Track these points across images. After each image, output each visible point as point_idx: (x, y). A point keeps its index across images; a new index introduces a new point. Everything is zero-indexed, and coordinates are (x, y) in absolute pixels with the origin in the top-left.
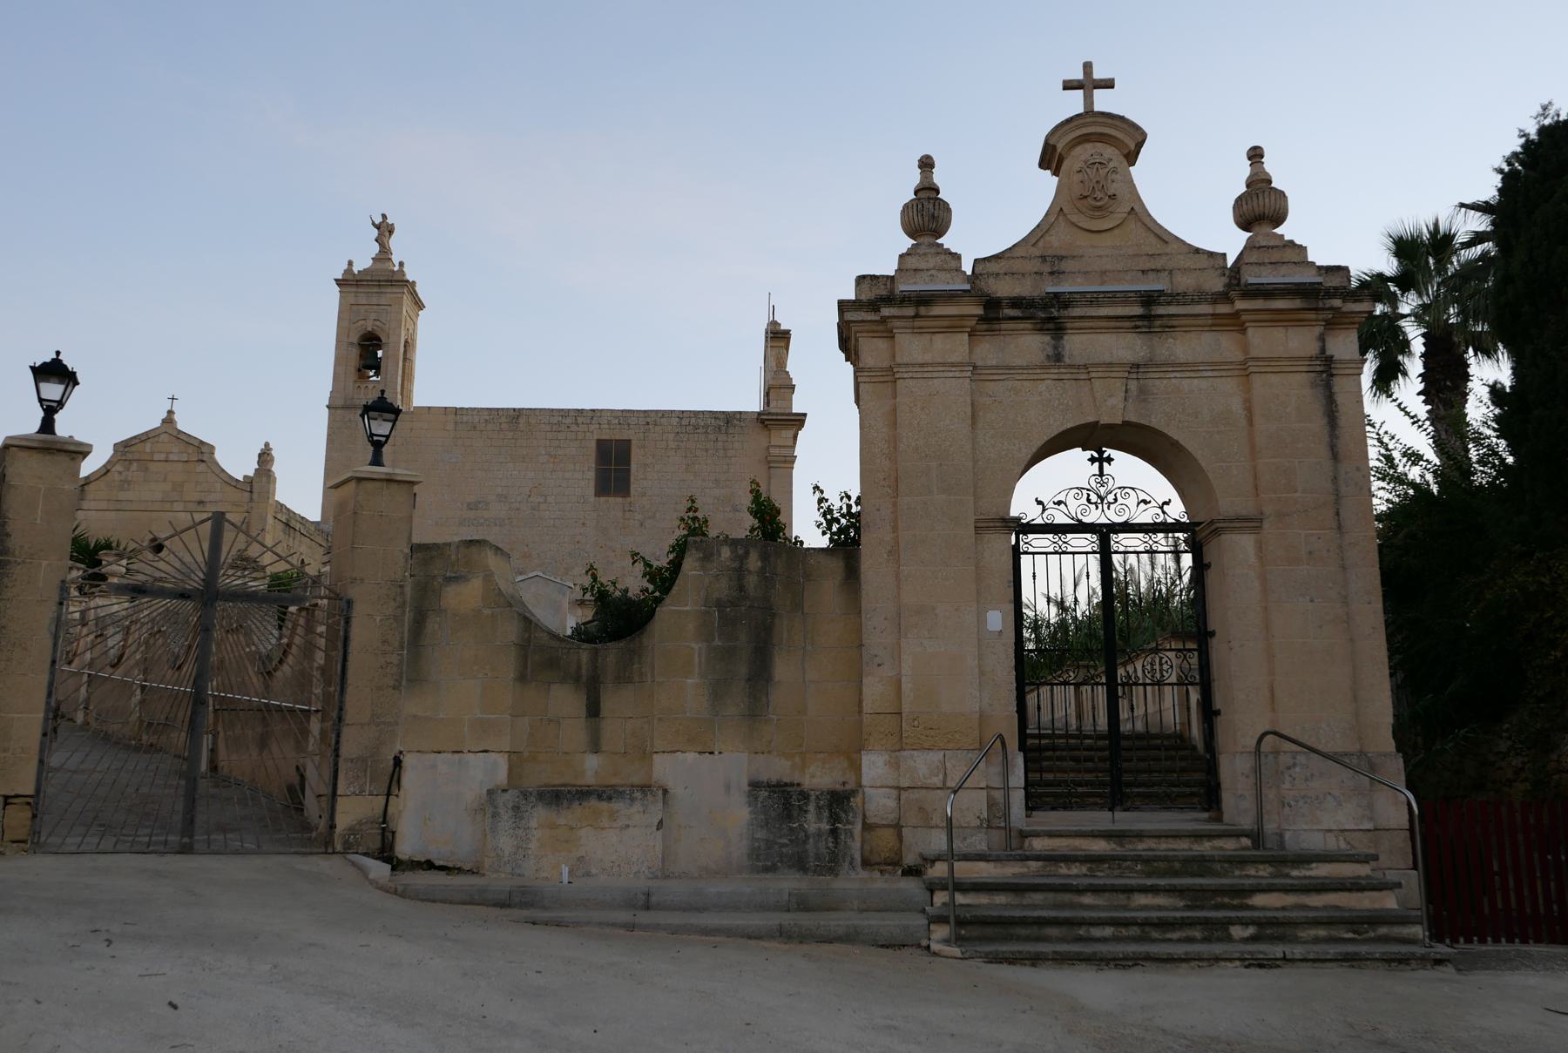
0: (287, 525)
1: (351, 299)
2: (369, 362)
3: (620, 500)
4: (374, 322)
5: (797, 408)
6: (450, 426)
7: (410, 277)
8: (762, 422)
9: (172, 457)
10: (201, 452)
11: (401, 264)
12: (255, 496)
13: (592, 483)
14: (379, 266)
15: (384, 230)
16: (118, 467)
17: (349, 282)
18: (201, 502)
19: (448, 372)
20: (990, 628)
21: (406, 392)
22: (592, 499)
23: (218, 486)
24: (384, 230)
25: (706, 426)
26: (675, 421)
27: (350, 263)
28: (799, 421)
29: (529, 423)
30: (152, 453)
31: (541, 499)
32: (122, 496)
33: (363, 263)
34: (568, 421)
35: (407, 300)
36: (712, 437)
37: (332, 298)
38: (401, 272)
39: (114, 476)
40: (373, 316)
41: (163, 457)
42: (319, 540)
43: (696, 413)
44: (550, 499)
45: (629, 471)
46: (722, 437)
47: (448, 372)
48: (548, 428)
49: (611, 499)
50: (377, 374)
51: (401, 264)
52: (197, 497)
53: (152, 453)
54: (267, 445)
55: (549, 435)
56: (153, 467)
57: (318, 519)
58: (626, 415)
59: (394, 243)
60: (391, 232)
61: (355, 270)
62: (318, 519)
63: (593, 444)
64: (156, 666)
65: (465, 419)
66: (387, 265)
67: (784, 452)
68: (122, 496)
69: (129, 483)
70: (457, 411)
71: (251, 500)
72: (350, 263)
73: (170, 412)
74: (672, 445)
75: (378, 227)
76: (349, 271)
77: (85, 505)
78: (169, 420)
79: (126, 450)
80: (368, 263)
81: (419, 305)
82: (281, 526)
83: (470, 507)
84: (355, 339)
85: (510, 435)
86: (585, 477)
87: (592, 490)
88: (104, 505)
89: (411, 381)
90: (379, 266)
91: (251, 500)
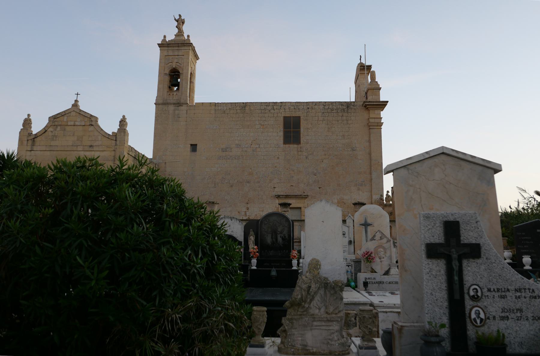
2: (174, 83)
3: (296, 146)
4: (175, 77)
6: (213, 112)
8: (365, 107)
9: (77, 123)
10: (91, 121)
11: (188, 36)
12: (118, 142)
13: (282, 138)
14: (178, 38)
15: (180, 22)
16: (51, 129)
17: (164, 45)
18: (91, 146)
19: (209, 86)
21: (191, 97)
23: (100, 137)
24: (180, 22)
25: (337, 109)
26: (322, 107)
27: (165, 37)
29: (250, 110)
30: (67, 121)
32: (53, 143)
33: (171, 37)
34: (270, 108)
35: (191, 53)
36: (340, 114)
38: (188, 39)
39: (49, 133)
40: (176, 61)
41: (72, 123)
44: (262, 146)
47: (209, 86)
49: (291, 146)
51: (188, 36)
52: (89, 143)
53: (67, 121)
54: (124, 116)
56: (68, 128)
57: (152, 157)
58: (297, 105)
60: (183, 23)
61: (167, 40)
62: (152, 157)
63: (282, 119)
65: (220, 108)
66: (182, 38)
67: (377, 121)
68: (53, 143)
70: (216, 104)
71: (116, 145)
72: (165, 37)
73: (76, 101)
74: (321, 118)
75: (177, 21)
77: (35, 148)
78: (76, 105)
79: (54, 119)
80: (173, 37)
81: (197, 57)
83: (224, 150)
84: (167, 72)
87: (282, 141)
89: (193, 92)
90: (178, 38)
91: (116, 145)
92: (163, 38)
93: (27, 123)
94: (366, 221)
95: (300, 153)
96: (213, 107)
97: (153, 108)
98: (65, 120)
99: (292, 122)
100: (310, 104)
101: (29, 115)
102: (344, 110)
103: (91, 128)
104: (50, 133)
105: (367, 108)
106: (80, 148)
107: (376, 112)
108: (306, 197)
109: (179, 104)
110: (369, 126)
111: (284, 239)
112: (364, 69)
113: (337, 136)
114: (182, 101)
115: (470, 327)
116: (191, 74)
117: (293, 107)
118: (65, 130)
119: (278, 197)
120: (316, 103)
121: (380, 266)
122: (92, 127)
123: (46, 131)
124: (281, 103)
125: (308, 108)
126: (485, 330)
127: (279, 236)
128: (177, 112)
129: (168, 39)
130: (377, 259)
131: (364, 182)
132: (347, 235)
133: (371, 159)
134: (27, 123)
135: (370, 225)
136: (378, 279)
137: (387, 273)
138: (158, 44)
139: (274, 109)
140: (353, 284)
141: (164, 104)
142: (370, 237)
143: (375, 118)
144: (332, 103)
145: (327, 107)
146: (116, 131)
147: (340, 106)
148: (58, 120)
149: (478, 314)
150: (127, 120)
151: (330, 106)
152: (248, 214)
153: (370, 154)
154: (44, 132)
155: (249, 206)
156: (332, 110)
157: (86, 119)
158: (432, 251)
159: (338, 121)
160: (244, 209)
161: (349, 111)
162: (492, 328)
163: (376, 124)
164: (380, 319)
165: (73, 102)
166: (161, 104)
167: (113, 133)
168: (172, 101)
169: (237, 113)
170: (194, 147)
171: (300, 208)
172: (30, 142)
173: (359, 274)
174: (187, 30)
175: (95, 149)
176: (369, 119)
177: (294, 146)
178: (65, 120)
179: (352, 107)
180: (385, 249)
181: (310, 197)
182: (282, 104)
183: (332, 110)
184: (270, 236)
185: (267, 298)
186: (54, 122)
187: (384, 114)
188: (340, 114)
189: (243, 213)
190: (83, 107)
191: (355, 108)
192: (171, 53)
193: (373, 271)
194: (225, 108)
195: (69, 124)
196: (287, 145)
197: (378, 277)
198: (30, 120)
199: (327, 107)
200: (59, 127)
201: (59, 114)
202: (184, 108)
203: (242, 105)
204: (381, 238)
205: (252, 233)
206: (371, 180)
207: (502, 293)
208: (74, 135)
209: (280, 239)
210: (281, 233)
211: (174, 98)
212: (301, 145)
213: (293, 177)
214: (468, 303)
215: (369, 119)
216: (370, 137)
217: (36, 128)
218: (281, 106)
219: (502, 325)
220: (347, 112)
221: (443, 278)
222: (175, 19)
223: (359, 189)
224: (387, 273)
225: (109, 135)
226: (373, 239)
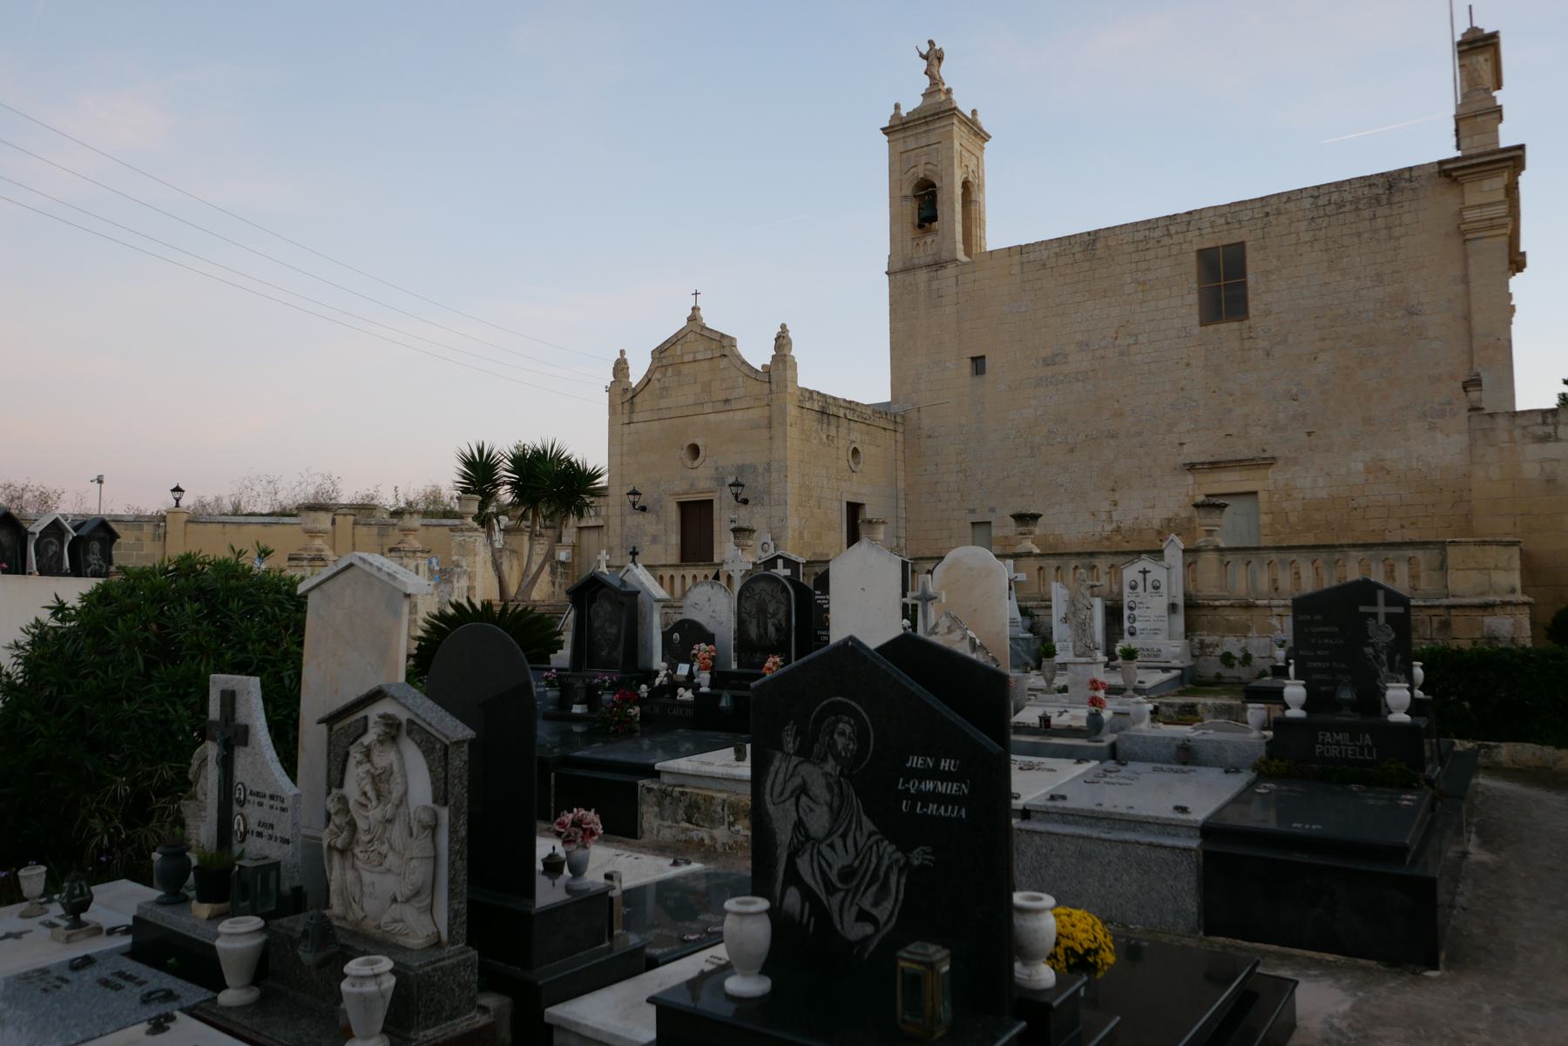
1: (900, 147)
3: (1235, 325)
4: (927, 205)
6: (1016, 269)
9: (700, 356)
10: (722, 345)
12: (774, 387)
13: (1195, 310)
14: (931, 100)
15: (933, 57)
16: (657, 375)
17: (897, 128)
18: (727, 401)
20: (730, 1015)
22: (1197, 330)
24: (933, 57)
25: (1356, 200)
26: (1307, 203)
27: (897, 107)
28: (1515, 159)
29: (1108, 247)
31: (1131, 341)
32: (664, 403)
33: (911, 102)
36: (1367, 214)
39: (655, 384)
40: (924, 160)
42: (883, 423)
45: (1244, 285)
46: (1381, 212)
47: (1021, 206)
48: (1132, 248)
49: (1223, 326)
52: (722, 396)
54: (783, 326)
55: (1135, 257)
56: (686, 369)
59: (946, 71)
60: (940, 59)
63: (1193, 257)
64: (40, 710)
65: (1032, 257)
68: (664, 403)
70: (1022, 249)
72: (897, 107)
75: (925, 57)
76: (896, 116)
78: (694, 317)
79: (660, 353)
81: (982, 136)
82: (811, 420)
84: (908, 190)
85: (1086, 265)
86: (1185, 300)
87: (1196, 319)
88: (648, 416)
89: (981, 224)
90: (931, 100)
93: (621, 368)
95: (1247, 344)
96: (1017, 258)
97: (884, 282)
100: (1273, 201)
101: (622, 352)
102: (1377, 198)
103: (724, 363)
105: (1455, 180)
106: (708, 408)
108: (1269, 462)
109: (937, 265)
110: (1463, 233)
111: (778, 629)
113: (1358, 278)
114: (945, 255)
116: (966, 185)
117: (1223, 220)
119: (1191, 467)
120: (1289, 196)
124: (1190, 213)
125: (1267, 214)
127: (770, 622)
128: (935, 285)
131: (1449, 403)
132: (1164, 589)
133: (1470, 332)
134: (621, 368)
135: (932, 598)
139: (1169, 235)
141: (904, 270)
143: (1481, 206)
144: (1338, 185)
145: (1323, 201)
147: (1366, 191)
151: (1335, 197)
152: (1115, 517)
153: (1467, 318)
155: (1117, 496)
156: (1340, 205)
159: (1359, 235)
160: (1106, 506)
161: (1395, 199)
163: (1487, 223)
165: (689, 313)
168: (923, 261)
169: (1075, 262)
170: (978, 363)
171: (1255, 493)
172: (627, 406)
174: (948, 73)
175: (734, 405)
176: (1461, 211)
177: (1228, 328)
179: (1403, 184)
181: (1280, 462)
184: (754, 622)
185: (611, 757)
186: (660, 359)
188: (1367, 214)
189: (1104, 516)
190: (711, 320)
191: (1415, 184)
192: (912, 144)
194: (1045, 254)
195: (686, 359)
196: (1211, 328)
198: (625, 362)
199: (1323, 201)
202: (950, 271)
203: (1086, 238)
204: (950, 630)
209: (771, 630)
210: (774, 616)
211: (930, 246)
212: (1252, 321)
213: (1230, 411)
215: (1461, 211)
216: (1466, 266)
217: (636, 376)
218: (1189, 223)
220: (1390, 203)
222: (921, 55)
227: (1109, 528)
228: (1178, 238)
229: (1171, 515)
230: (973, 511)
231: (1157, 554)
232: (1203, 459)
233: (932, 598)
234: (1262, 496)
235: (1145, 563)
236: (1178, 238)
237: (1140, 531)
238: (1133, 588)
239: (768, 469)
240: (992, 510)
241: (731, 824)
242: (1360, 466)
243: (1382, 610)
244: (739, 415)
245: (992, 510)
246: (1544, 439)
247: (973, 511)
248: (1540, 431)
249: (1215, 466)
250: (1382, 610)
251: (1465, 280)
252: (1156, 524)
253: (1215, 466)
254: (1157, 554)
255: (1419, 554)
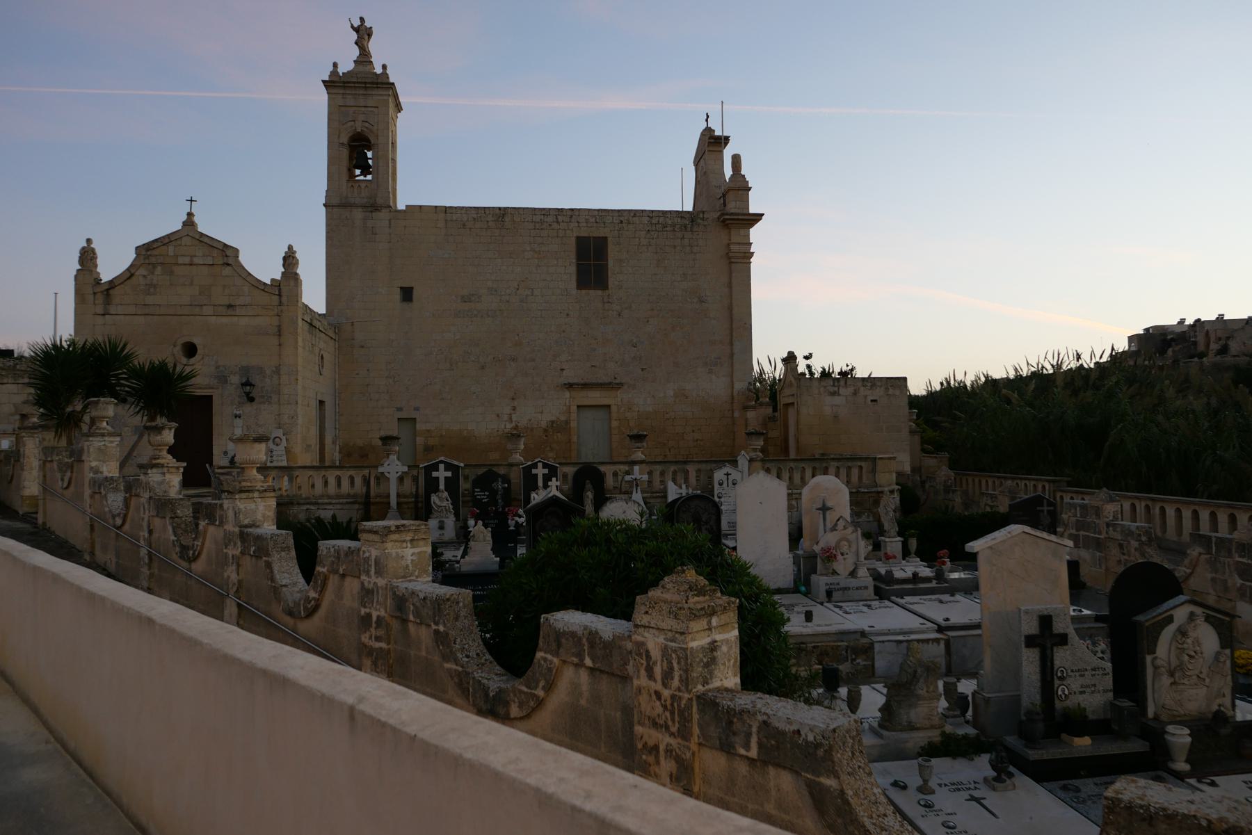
0: (311, 324)
3: (600, 292)
5: (753, 209)
7: (391, 80)
9: (196, 260)
10: (226, 255)
11: (384, 67)
12: (284, 299)
13: (574, 278)
14: (361, 68)
15: (363, 33)
16: (142, 271)
18: (230, 306)
19: (427, 175)
22: (574, 292)
24: (363, 33)
25: (674, 225)
26: (645, 220)
27: (335, 65)
30: (176, 256)
32: (150, 300)
33: (346, 66)
34: (550, 219)
36: (679, 235)
37: (323, 96)
38: (385, 74)
40: (361, 117)
41: (187, 260)
43: (664, 213)
46: (688, 235)
47: (427, 175)
49: (592, 292)
50: (364, 173)
51: (384, 67)
53: (176, 256)
54: (290, 247)
59: (373, 46)
60: (370, 35)
63: (573, 241)
65: (454, 217)
66: (368, 68)
67: (743, 248)
68: (150, 300)
69: (155, 286)
70: (446, 209)
71: (281, 304)
72: (335, 65)
73: (190, 215)
75: (357, 30)
76: (334, 73)
77: (112, 310)
78: (189, 222)
79: (145, 251)
81: (399, 108)
82: (306, 327)
83: (466, 299)
86: (567, 271)
87: (574, 283)
88: (132, 309)
91: (281, 304)
92: (331, 68)
93: (88, 256)
94: (824, 505)
97: (322, 212)
98: (171, 252)
99: (592, 246)
101: (89, 241)
104: (141, 279)
106: (208, 310)
107: (742, 231)
108: (619, 386)
112: (712, 143)
115: (1057, 702)
118: (172, 273)
119: (570, 386)
121: (842, 566)
122: (229, 268)
123: (132, 275)
126: (1068, 703)
129: (342, 70)
130: (840, 557)
134: (88, 256)
135: (829, 509)
136: (842, 585)
137: (853, 574)
138: (324, 82)
140: (803, 589)
142: (829, 525)
146: (278, 277)
148: (154, 252)
149: (1063, 691)
150: (297, 255)
151: (661, 220)
152: (514, 419)
153: (730, 309)
154: (129, 278)
156: (665, 226)
157: (215, 253)
158: (1030, 641)
160: (508, 410)
161: (695, 229)
162: (1072, 702)
164: (876, 650)
165: (185, 218)
166: (335, 206)
167: (272, 280)
169: (488, 228)
170: (407, 294)
171: (609, 406)
173: (814, 577)
177: (595, 293)
178: (171, 252)
180: (848, 541)
182: (573, 214)
183: (665, 226)
187: (755, 233)
189: (506, 417)
193: (835, 573)
195: (181, 260)
196: (584, 292)
197: (843, 580)
198: (93, 250)
200: (159, 268)
201: (156, 240)
202: (384, 214)
205: (589, 486)
206: (732, 355)
207: (1081, 672)
208: (191, 284)
214: (1057, 682)
217: (110, 267)
219: (1080, 698)
221: (1037, 663)
222: (352, 27)
223: (710, 372)
224: (853, 574)
225: (265, 284)
226: (834, 529)
227: (509, 426)
228: (563, 226)
229: (554, 418)
230: (400, 409)
231: (734, 463)
232: (575, 381)
233: (829, 509)
234: (614, 409)
235: (728, 469)
236: (563, 226)
237: (532, 430)
238: (721, 484)
239: (277, 371)
240: (417, 409)
241: (853, 660)
242: (671, 393)
243: (1045, 508)
244: (244, 321)
245: (417, 409)
246: (834, 394)
247: (400, 409)
248: (832, 389)
249: (586, 386)
250: (1045, 508)
251: (730, 285)
252: (544, 424)
253: (586, 386)
254: (734, 463)
255: (863, 464)
